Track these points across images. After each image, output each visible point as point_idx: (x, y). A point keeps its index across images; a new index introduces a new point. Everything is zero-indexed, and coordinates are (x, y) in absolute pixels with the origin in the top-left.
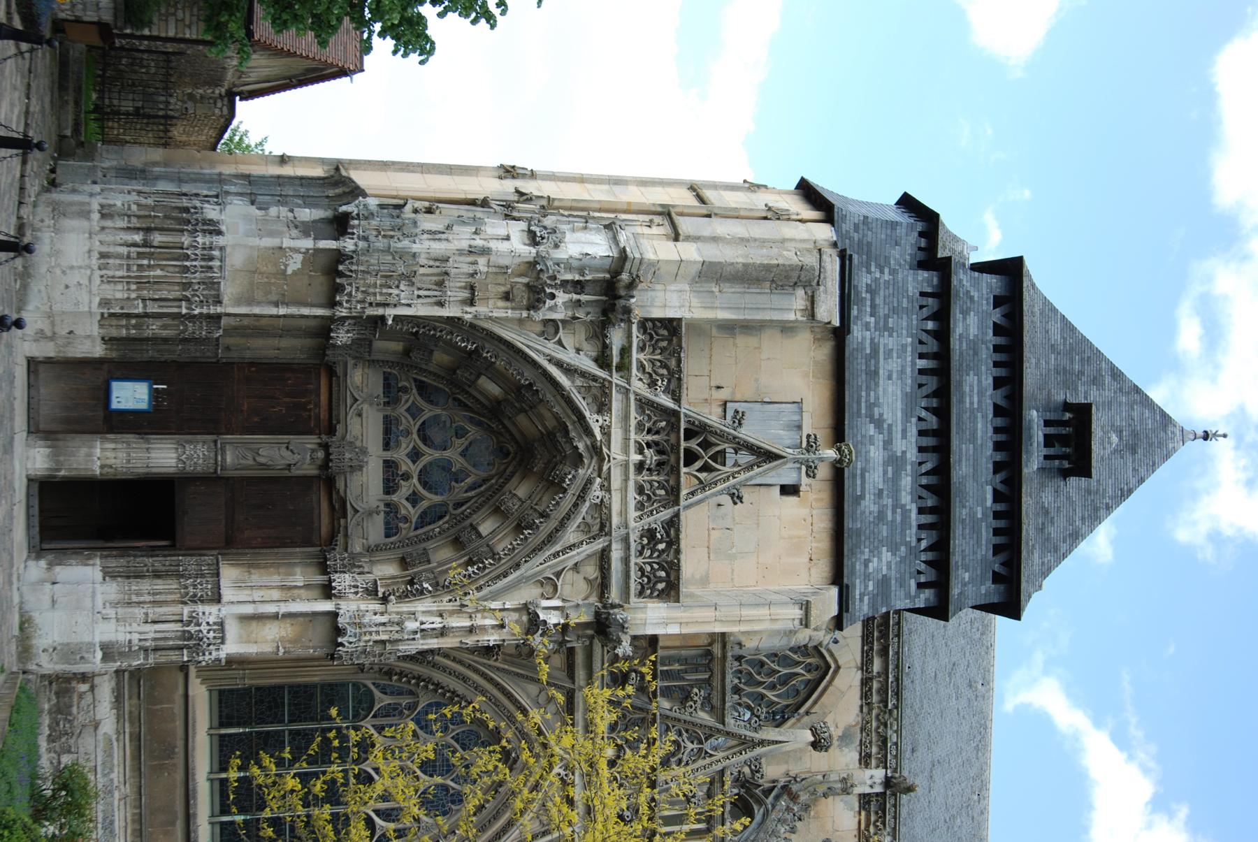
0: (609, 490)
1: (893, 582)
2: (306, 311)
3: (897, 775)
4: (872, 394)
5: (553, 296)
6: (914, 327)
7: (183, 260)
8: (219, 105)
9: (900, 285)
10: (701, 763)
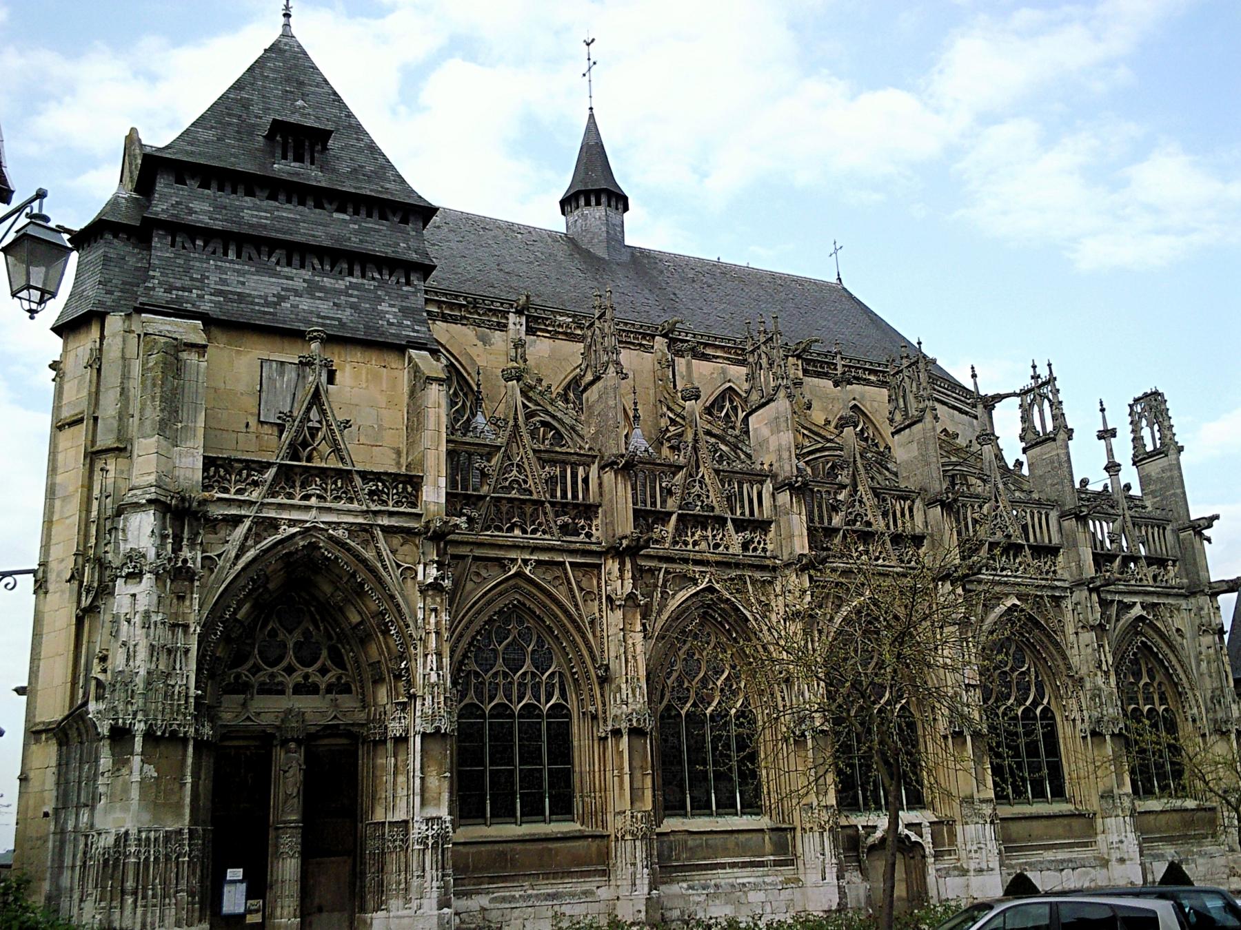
0: (339, 524)
1: (404, 304)
2: (190, 761)
4: (257, 300)
5: (185, 561)
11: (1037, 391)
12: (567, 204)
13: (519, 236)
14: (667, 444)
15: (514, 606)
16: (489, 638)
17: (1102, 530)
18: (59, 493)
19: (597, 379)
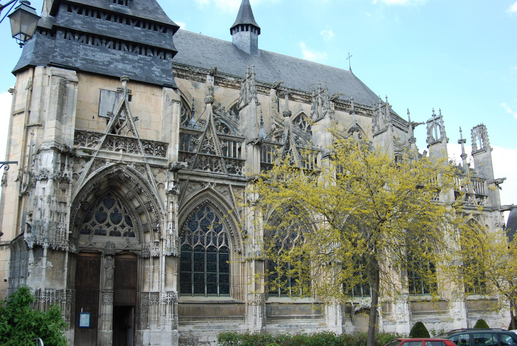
0: (131, 162)
2: (66, 261)
3: (210, 71)
4: (100, 63)
5: (66, 175)
9: (61, 45)
10: (214, 141)
11: (434, 121)
12: (233, 29)
13: (212, 42)
14: (274, 136)
15: (206, 203)
16: (195, 216)
17: (459, 182)
18: (13, 143)
19: (247, 104)
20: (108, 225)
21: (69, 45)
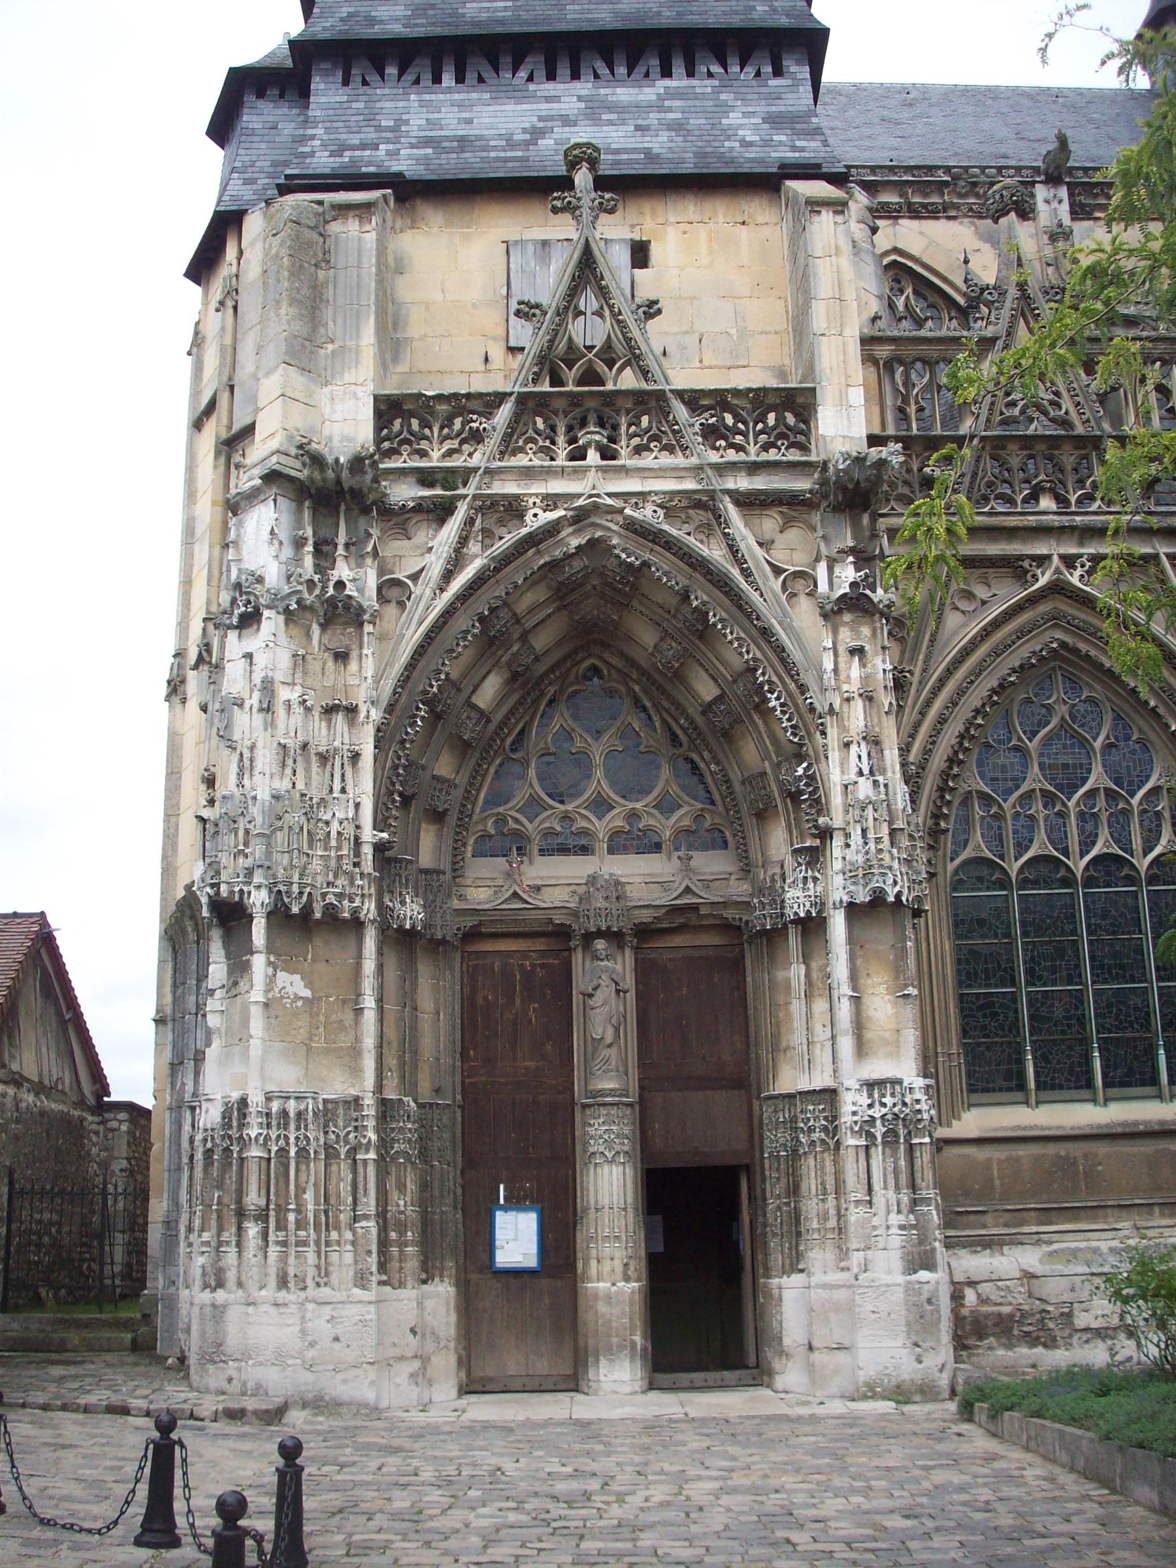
0: (643, 495)
1: (774, 109)
2: (369, 966)
4: (492, 143)
5: (340, 585)
6: (395, 91)
7: (288, 1158)
8: (114, 1124)
20: (601, 806)
21: (361, 105)
